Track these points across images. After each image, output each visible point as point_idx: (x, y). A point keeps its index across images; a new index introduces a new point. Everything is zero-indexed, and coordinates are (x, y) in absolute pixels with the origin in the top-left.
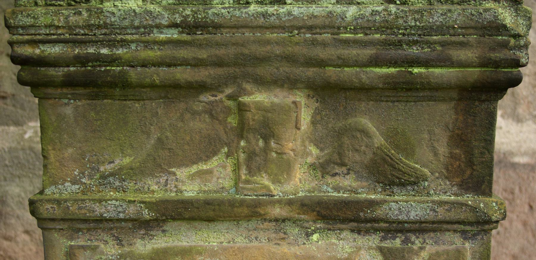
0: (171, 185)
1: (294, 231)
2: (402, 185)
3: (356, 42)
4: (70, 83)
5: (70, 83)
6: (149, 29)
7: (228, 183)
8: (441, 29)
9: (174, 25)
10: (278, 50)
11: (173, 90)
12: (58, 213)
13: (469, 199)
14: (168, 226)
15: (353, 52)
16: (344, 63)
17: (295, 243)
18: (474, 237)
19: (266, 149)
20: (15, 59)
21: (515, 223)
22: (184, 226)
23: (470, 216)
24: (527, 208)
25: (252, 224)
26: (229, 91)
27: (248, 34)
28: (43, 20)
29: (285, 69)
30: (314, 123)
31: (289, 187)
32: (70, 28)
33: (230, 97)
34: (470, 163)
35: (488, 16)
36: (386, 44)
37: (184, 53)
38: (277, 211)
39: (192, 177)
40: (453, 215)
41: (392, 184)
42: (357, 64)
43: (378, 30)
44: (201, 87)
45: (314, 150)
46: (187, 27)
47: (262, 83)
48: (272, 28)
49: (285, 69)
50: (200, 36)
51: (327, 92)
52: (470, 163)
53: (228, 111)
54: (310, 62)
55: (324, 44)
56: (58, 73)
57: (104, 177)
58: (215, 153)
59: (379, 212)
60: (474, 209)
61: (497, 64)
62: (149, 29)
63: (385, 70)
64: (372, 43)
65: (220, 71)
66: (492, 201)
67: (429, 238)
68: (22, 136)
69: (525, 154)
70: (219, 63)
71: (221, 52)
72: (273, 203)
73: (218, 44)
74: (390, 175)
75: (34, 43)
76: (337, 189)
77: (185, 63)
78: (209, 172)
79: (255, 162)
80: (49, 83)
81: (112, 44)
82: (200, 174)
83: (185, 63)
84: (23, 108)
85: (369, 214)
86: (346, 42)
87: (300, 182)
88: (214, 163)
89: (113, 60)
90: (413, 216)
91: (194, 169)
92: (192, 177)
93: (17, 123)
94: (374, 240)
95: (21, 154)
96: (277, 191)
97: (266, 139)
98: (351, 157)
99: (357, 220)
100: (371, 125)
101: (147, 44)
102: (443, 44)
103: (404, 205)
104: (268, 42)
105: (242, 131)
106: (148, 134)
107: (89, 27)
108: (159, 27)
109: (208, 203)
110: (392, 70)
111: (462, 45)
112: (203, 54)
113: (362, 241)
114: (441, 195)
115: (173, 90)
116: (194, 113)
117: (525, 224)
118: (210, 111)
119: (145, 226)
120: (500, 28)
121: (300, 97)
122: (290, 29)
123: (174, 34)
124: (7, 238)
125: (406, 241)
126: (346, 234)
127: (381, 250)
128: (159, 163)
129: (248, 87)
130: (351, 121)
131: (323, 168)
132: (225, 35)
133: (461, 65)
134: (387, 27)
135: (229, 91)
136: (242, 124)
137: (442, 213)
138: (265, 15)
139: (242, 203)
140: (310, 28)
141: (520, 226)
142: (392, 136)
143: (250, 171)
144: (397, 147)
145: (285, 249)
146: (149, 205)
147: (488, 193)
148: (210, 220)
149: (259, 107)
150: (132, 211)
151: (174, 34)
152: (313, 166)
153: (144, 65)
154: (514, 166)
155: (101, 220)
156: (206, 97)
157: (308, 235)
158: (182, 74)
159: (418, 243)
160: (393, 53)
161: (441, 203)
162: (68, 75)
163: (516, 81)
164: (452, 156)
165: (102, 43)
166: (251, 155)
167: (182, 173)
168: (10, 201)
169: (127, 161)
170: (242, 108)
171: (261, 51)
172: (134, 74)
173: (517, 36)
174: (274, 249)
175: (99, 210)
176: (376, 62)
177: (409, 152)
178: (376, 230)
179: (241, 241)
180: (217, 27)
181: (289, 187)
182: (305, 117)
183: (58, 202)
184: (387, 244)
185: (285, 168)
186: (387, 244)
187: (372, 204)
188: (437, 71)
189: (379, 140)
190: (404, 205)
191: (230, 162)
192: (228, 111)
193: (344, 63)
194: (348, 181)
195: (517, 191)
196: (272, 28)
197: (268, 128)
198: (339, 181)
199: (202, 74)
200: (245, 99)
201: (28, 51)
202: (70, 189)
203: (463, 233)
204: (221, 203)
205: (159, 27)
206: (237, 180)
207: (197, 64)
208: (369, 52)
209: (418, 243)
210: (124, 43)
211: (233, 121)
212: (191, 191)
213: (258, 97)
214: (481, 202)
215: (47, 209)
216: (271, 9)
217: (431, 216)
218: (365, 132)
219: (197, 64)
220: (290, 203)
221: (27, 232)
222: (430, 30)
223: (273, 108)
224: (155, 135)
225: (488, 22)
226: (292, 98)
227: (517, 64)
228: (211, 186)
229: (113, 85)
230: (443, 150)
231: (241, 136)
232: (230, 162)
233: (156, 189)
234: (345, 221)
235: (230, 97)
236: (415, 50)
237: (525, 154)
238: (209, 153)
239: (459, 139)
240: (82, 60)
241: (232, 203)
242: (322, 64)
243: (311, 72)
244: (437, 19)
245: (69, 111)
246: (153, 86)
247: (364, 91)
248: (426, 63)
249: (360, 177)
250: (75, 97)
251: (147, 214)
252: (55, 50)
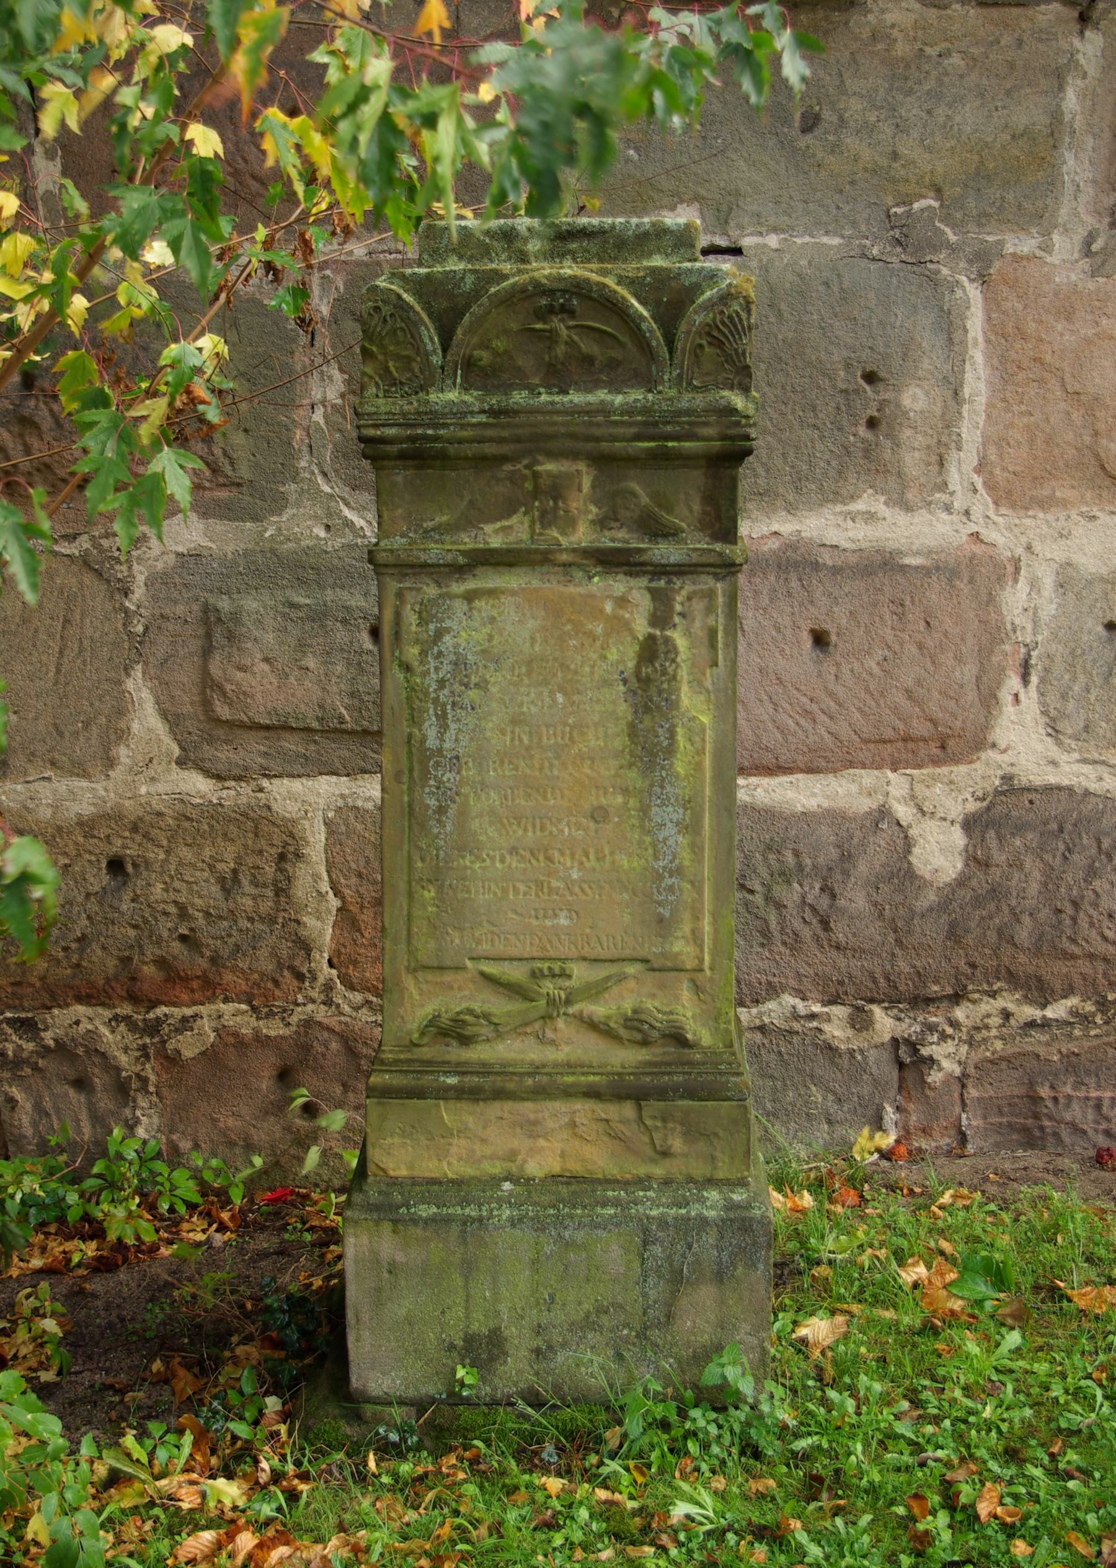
0: (480, 538)
1: (579, 574)
2: (665, 536)
3: (623, 423)
4: (402, 456)
5: (402, 456)
6: (464, 414)
7: (525, 536)
8: (688, 412)
9: (483, 412)
10: (563, 430)
11: (482, 462)
12: (391, 559)
13: (718, 547)
14: (479, 571)
15: (621, 430)
16: (614, 439)
17: (580, 584)
18: (723, 578)
19: (556, 508)
20: (361, 439)
21: (907, 646)
22: (490, 570)
23: (718, 560)
24: (922, 624)
25: (545, 569)
26: (525, 462)
27: (540, 418)
28: (383, 409)
29: (569, 444)
30: (593, 487)
31: (574, 539)
32: (404, 414)
33: (526, 467)
34: (719, 518)
35: (723, 402)
36: (645, 424)
37: (490, 433)
38: (564, 557)
39: (496, 532)
40: (704, 559)
41: (656, 535)
42: (623, 440)
43: (640, 413)
44: (504, 459)
45: (594, 509)
46: (493, 412)
47: (552, 455)
48: (558, 413)
49: (569, 444)
50: (503, 419)
51: (603, 462)
52: (719, 518)
53: (524, 478)
54: (588, 438)
55: (598, 425)
56: (393, 449)
57: (426, 532)
58: (515, 512)
59: (645, 558)
60: (720, 554)
61: (732, 438)
62: (464, 414)
63: (646, 444)
64: (634, 424)
65: (519, 446)
66: (737, 549)
67: (688, 579)
68: (261, 534)
69: (918, 553)
70: (518, 440)
71: (520, 431)
72: (561, 551)
73: (517, 426)
74: (656, 530)
75: (376, 426)
76: (613, 540)
77: (491, 440)
78: (510, 527)
79: (547, 518)
80: (387, 457)
81: (435, 426)
82: (504, 529)
83: (491, 440)
84: (263, 499)
85: (638, 558)
86: (615, 423)
87: (582, 535)
88: (514, 520)
89: (436, 439)
90: (672, 560)
91: (498, 525)
92: (496, 532)
93: (255, 518)
94: (643, 581)
95: (259, 558)
96: (564, 541)
97: (555, 500)
98: (624, 514)
99: (628, 564)
100: (640, 490)
101: (463, 427)
102: (690, 424)
103: (666, 552)
104: (555, 424)
105: (536, 494)
106: (462, 497)
107: (418, 413)
108: (472, 413)
109: (509, 551)
110: (652, 444)
111: (705, 424)
112: (505, 433)
113: (634, 582)
114: (694, 544)
115: (482, 462)
116: (498, 480)
117: (921, 646)
118: (512, 478)
119: (459, 570)
120: (732, 411)
121: (582, 466)
122: (572, 413)
123: (483, 418)
124: (241, 668)
125: (669, 582)
126: (620, 577)
127: (649, 589)
128: (469, 521)
129: (540, 458)
130: (623, 485)
131: (602, 523)
132: (522, 418)
133: (704, 439)
134: (646, 410)
135: (525, 462)
136: (536, 487)
137: (695, 558)
138: (552, 403)
139: (536, 551)
140: (588, 413)
141: (914, 650)
142: (656, 497)
143: (543, 527)
144: (660, 506)
145: (571, 589)
146: (463, 553)
147: (734, 542)
148: (511, 565)
149: (549, 474)
150: (449, 558)
151: (483, 418)
152: (593, 522)
153: (460, 442)
154: (904, 569)
155: (425, 565)
156: (508, 467)
157: (590, 578)
158: (489, 449)
159: (679, 584)
160: (651, 431)
161: (695, 550)
162: (401, 451)
163: (749, 452)
164: (704, 513)
165: (428, 426)
166: (544, 513)
167: (488, 528)
168: (245, 618)
169: (445, 518)
170: (536, 475)
171: (550, 430)
172: (452, 450)
173: (747, 417)
174: (562, 589)
175: (423, 557)
176: (638, 437)
177: (670, 510)
178: (645, 573)
179: (536, 583)
180: (516, 412)
181: (574, 539)
182: (586, 483)
183: (392, 551)
184: (654, 585)
185: (570, 523)
186: (654, 585)
187: (639, 551)
188: (687, 444)
189: (645, 500)
190: (666, 552)
191: (527, 519)
192: (524, 478)
193: (614, 439)
194: (622, 534)
195: (908, 602)
196: (558, 413)
197: (556, 490)
198: (613, 533)
199: (505, 449)
200: (539, 468)
201: (371, 432)
202: (399, 542)
203: (715, 575)
204: (519, 551)
205: (472, 413)
206: (533, 534)
207: (501, 441)
208: (634, 430)
209: (679, 584)
210: (445, 426)
211: (529, 486)
212: (496, 542)
213: (549, 467)
214: (727, 549)
215: (382, 557)
216: (557, 398)
217: (685, 560)
218: (633, 494)
219: (501, 441)
220: (574, 550)
221: (266, 660)
222: (680, 413)
223: (560, 476)
224: (467, 498)
225: (284, 497)
226: (574, 468)
227: (747, 438)
228: (511, 539)
229: (435, 458)
230: (697, 507)
231: (535, 498)
232: (527, 519)
233: (468, 541)
234: (619, 565)
235: (526, 467)
236: (669, 428)
237: (918, 553)
238: (510, 512)
239: (709, 499)
240: (412, 439)
241: (529, 551)
242: (597, 439)
243: (590, 446)
244: (684, 404)
245: (399, 479)
246: (466, 458)
247: (631, 460)
248: (678, 438)
249: (631, 531)
250: (405, 468)
251: (461, 560)
252: (391, 432)
